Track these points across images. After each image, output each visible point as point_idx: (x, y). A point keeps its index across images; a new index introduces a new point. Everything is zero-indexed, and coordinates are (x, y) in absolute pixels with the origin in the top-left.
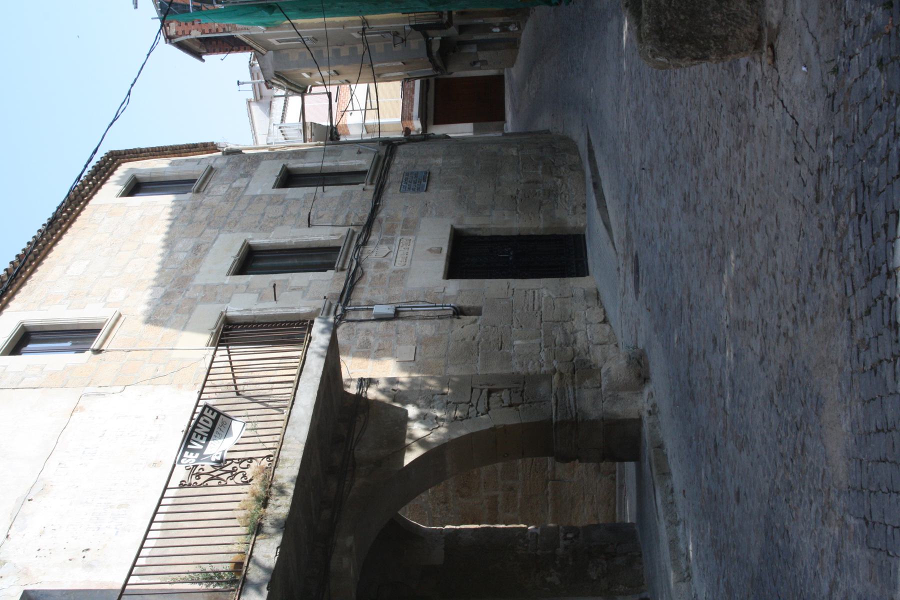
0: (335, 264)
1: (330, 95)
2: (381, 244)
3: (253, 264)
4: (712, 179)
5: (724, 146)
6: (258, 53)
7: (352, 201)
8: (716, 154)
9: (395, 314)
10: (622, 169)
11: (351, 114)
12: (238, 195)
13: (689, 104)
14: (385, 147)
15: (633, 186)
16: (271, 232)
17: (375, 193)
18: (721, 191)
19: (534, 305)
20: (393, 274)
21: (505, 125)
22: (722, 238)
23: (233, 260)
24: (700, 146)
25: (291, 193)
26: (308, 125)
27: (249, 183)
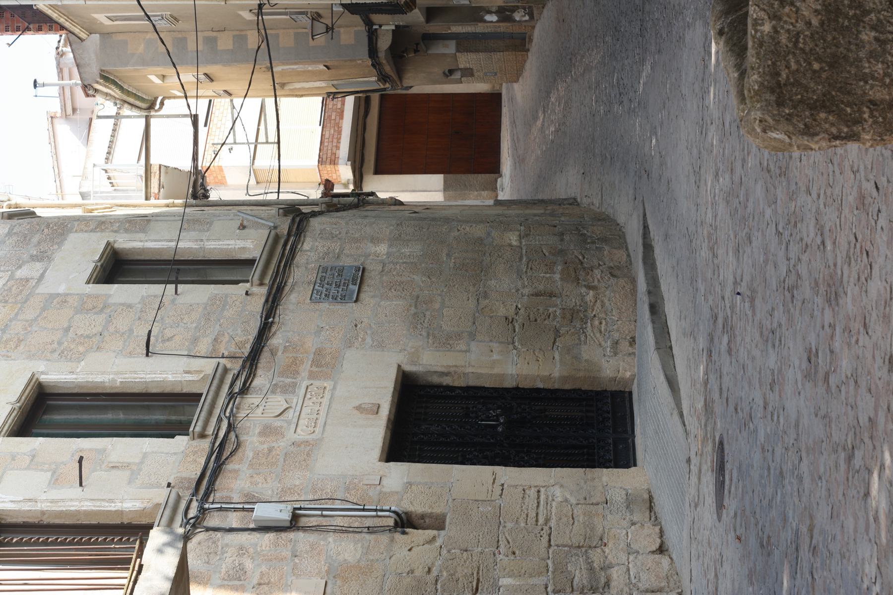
0: (190, 423)
1: (195, 120)
2: (273, 392)
3: (45, 417)
4: (859, 333)
5: (881, 281)
6: (72, 37)
7: (225, 313)
8: (866, 292)
9: (291, 521)
10: (702, 287)
11: (231, 150)
12: (26, 292)
13: (822, 196)
14: (289, 220)
15: (720, 321)
16: (79, 362)
17: (267, 301)
18: (874, 357)
19: (537, 514)
20: (292, 448)
21: (499, 180)
22: (871, 438)
23: (9, 408)
24: (839, 273)
25: (118, 292)
26: (155, 169)
27: (45, 271)
